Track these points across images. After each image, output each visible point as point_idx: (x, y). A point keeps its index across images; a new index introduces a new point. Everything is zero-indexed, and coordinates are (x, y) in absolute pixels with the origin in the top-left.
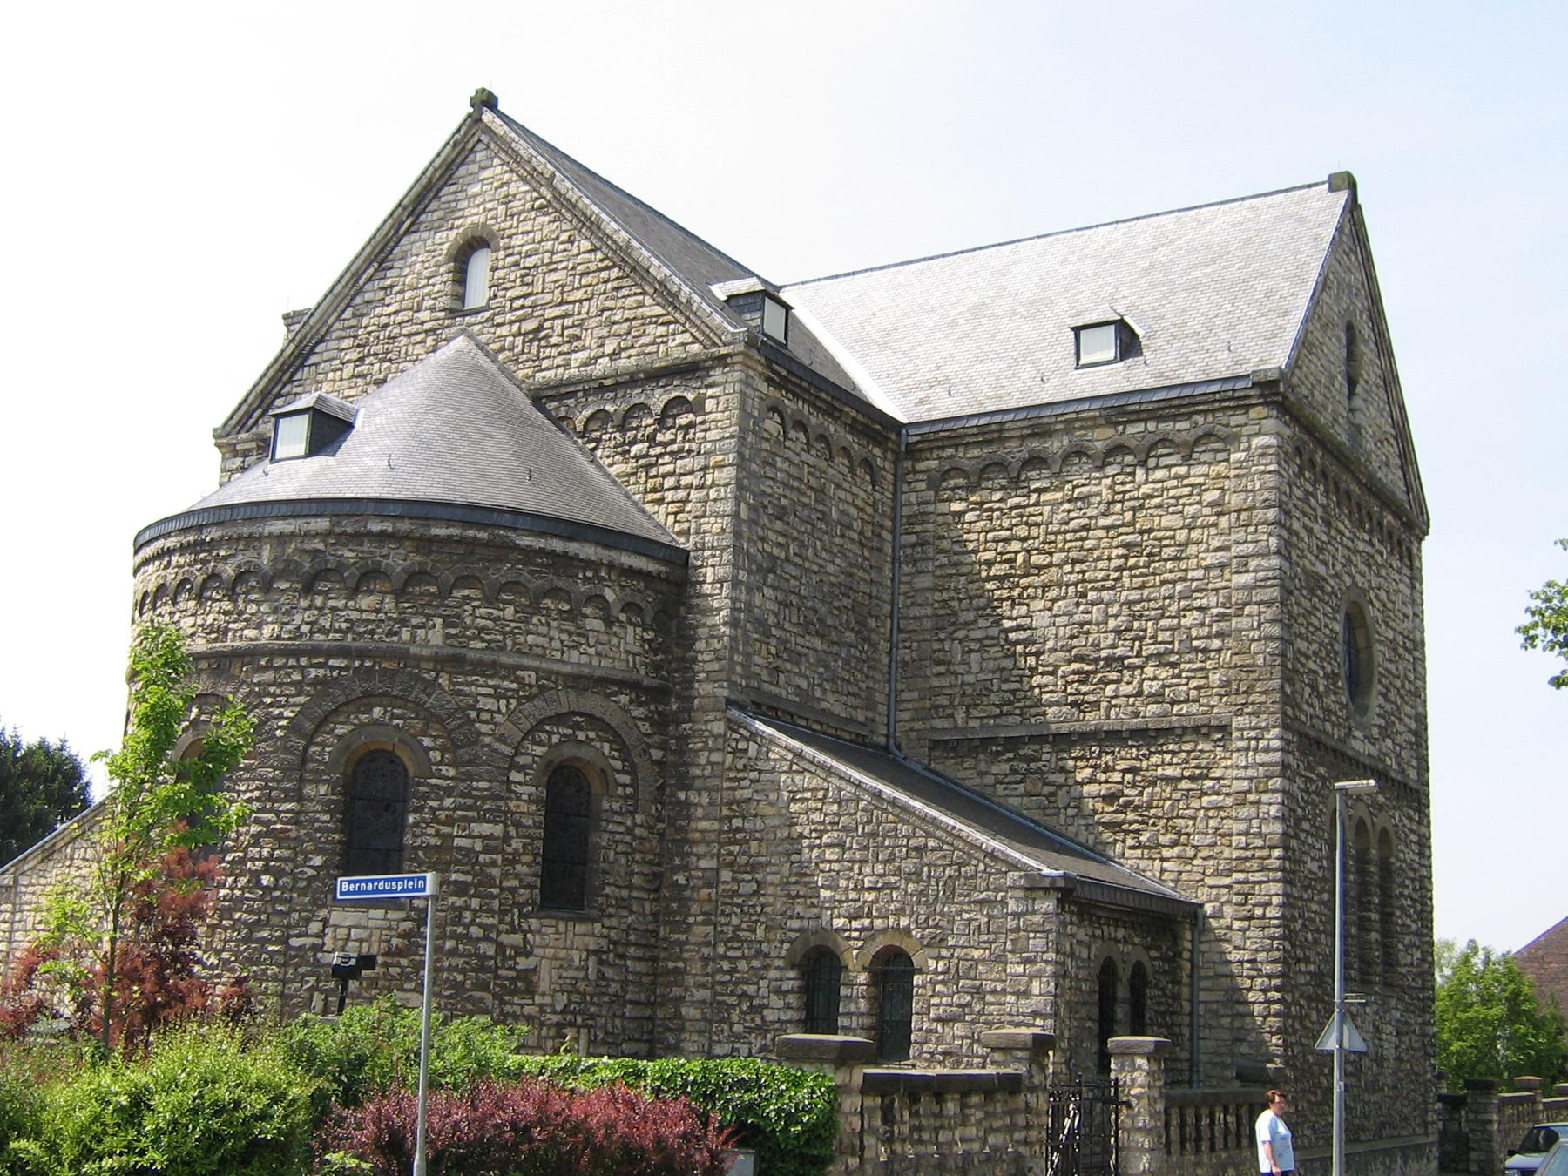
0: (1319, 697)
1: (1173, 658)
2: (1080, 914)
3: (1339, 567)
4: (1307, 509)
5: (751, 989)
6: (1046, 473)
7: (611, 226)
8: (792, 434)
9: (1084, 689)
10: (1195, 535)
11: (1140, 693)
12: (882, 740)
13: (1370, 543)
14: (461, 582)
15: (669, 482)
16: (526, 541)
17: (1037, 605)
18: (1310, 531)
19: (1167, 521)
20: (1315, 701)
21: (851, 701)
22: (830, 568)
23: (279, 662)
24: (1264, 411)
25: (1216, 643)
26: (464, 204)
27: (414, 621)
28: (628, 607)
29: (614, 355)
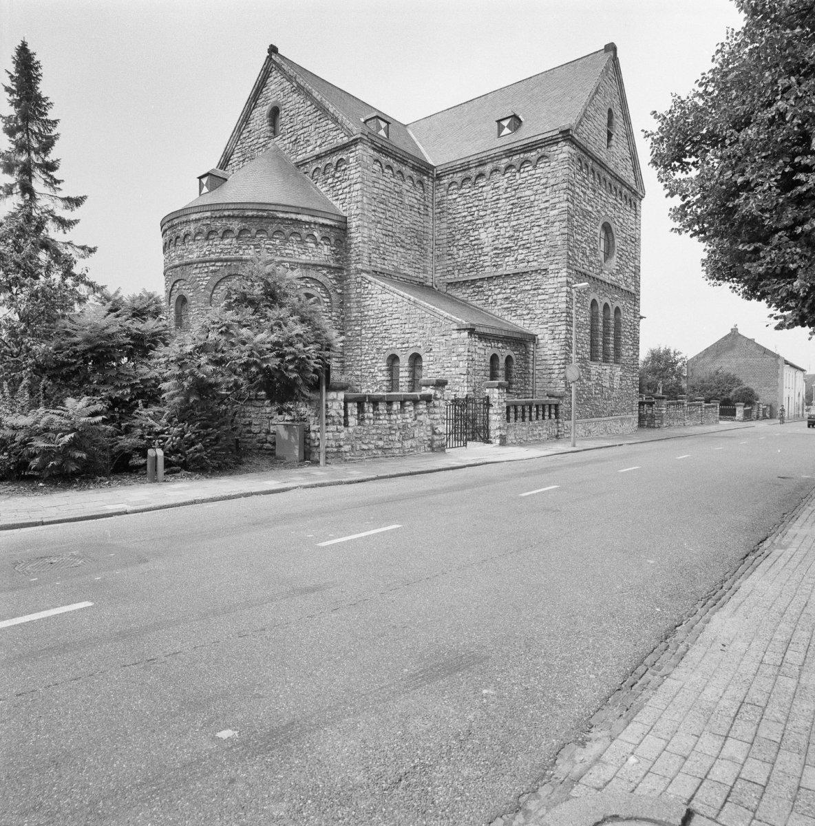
0: (587, 257)
1: (528, 245)
2: (480, 338)
3: (599, 208)
4: (583, 184)
5: (372, 370)
6: (485, 179)
7: (315, 94)
8: (386, 171)
9: (498, 260)
10: (537, 197)
11: (516, 260)
12: (431, 284)
13: (615, 199)
14: (259, 232)
15: (340, 192)
16: (281, 215)
17: (481, 230)
18: (585, 193)
19: (528, 193)
20: (585, 259)
21: (417, 270)
22: (406, 222)
23: (200, 265)
24: (564, 143)
25: (543, 238)
26: (270, 94)
27: (244, 247)
28: (324, 238)
29: (320, 146)
